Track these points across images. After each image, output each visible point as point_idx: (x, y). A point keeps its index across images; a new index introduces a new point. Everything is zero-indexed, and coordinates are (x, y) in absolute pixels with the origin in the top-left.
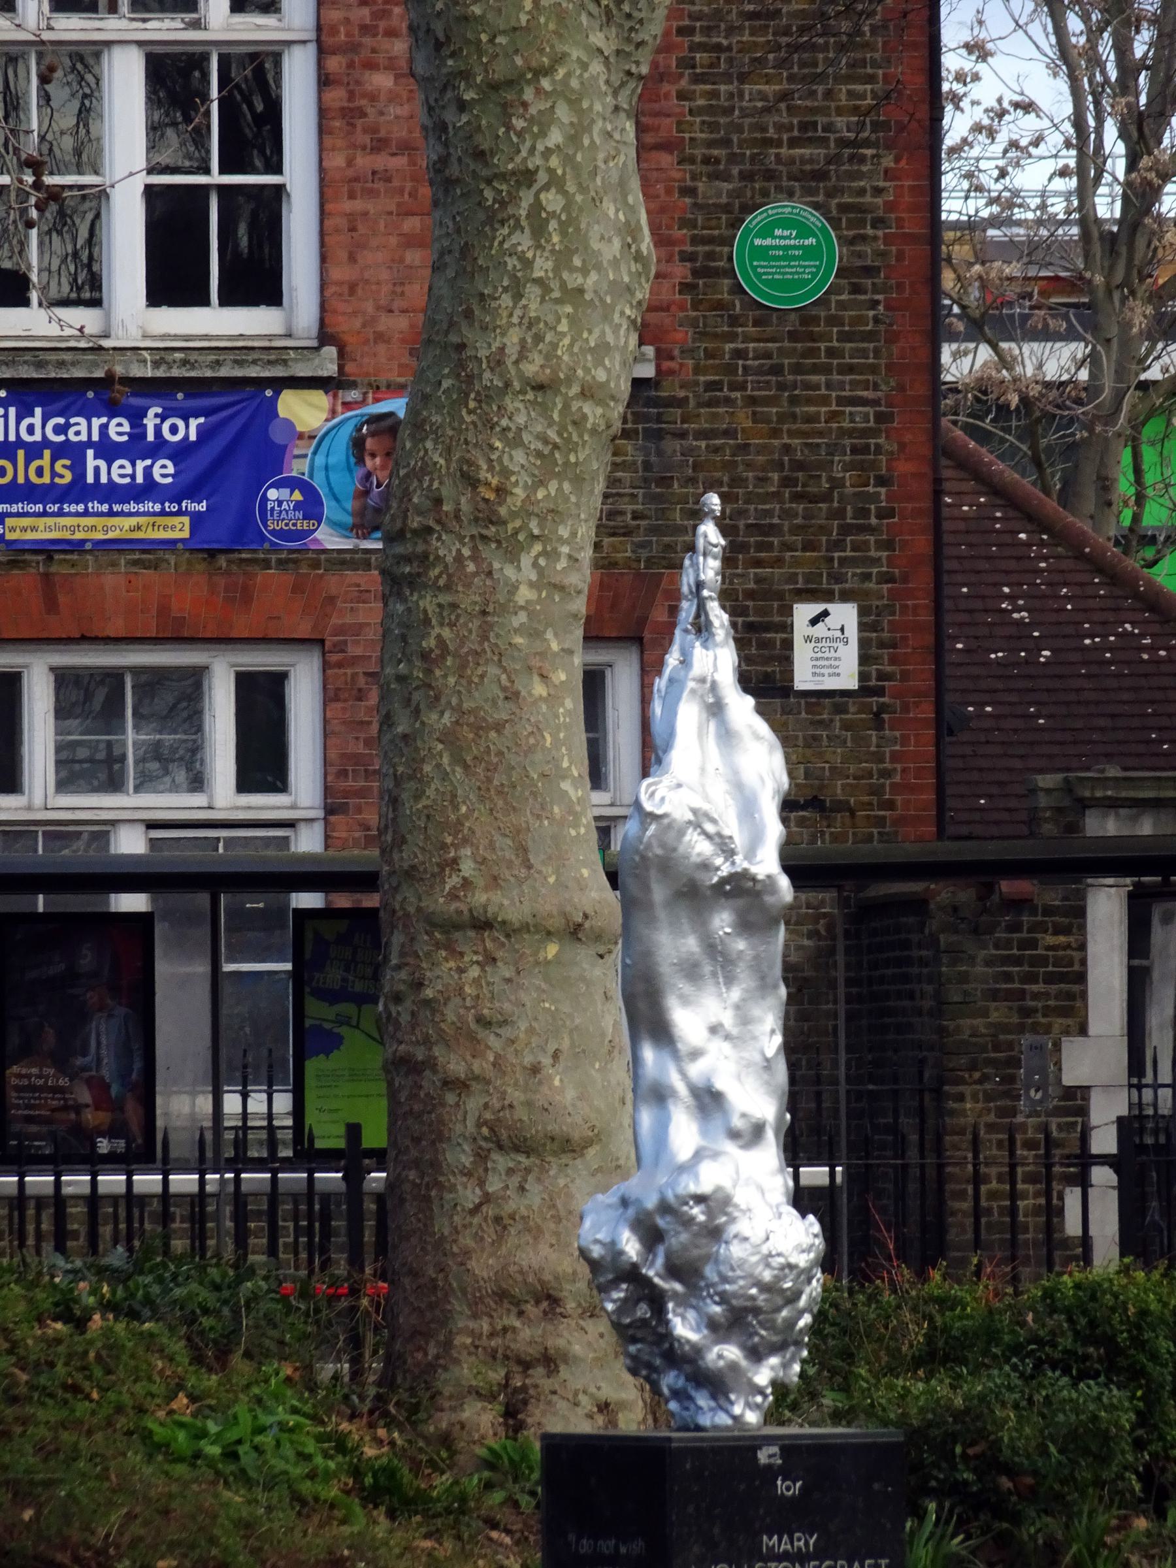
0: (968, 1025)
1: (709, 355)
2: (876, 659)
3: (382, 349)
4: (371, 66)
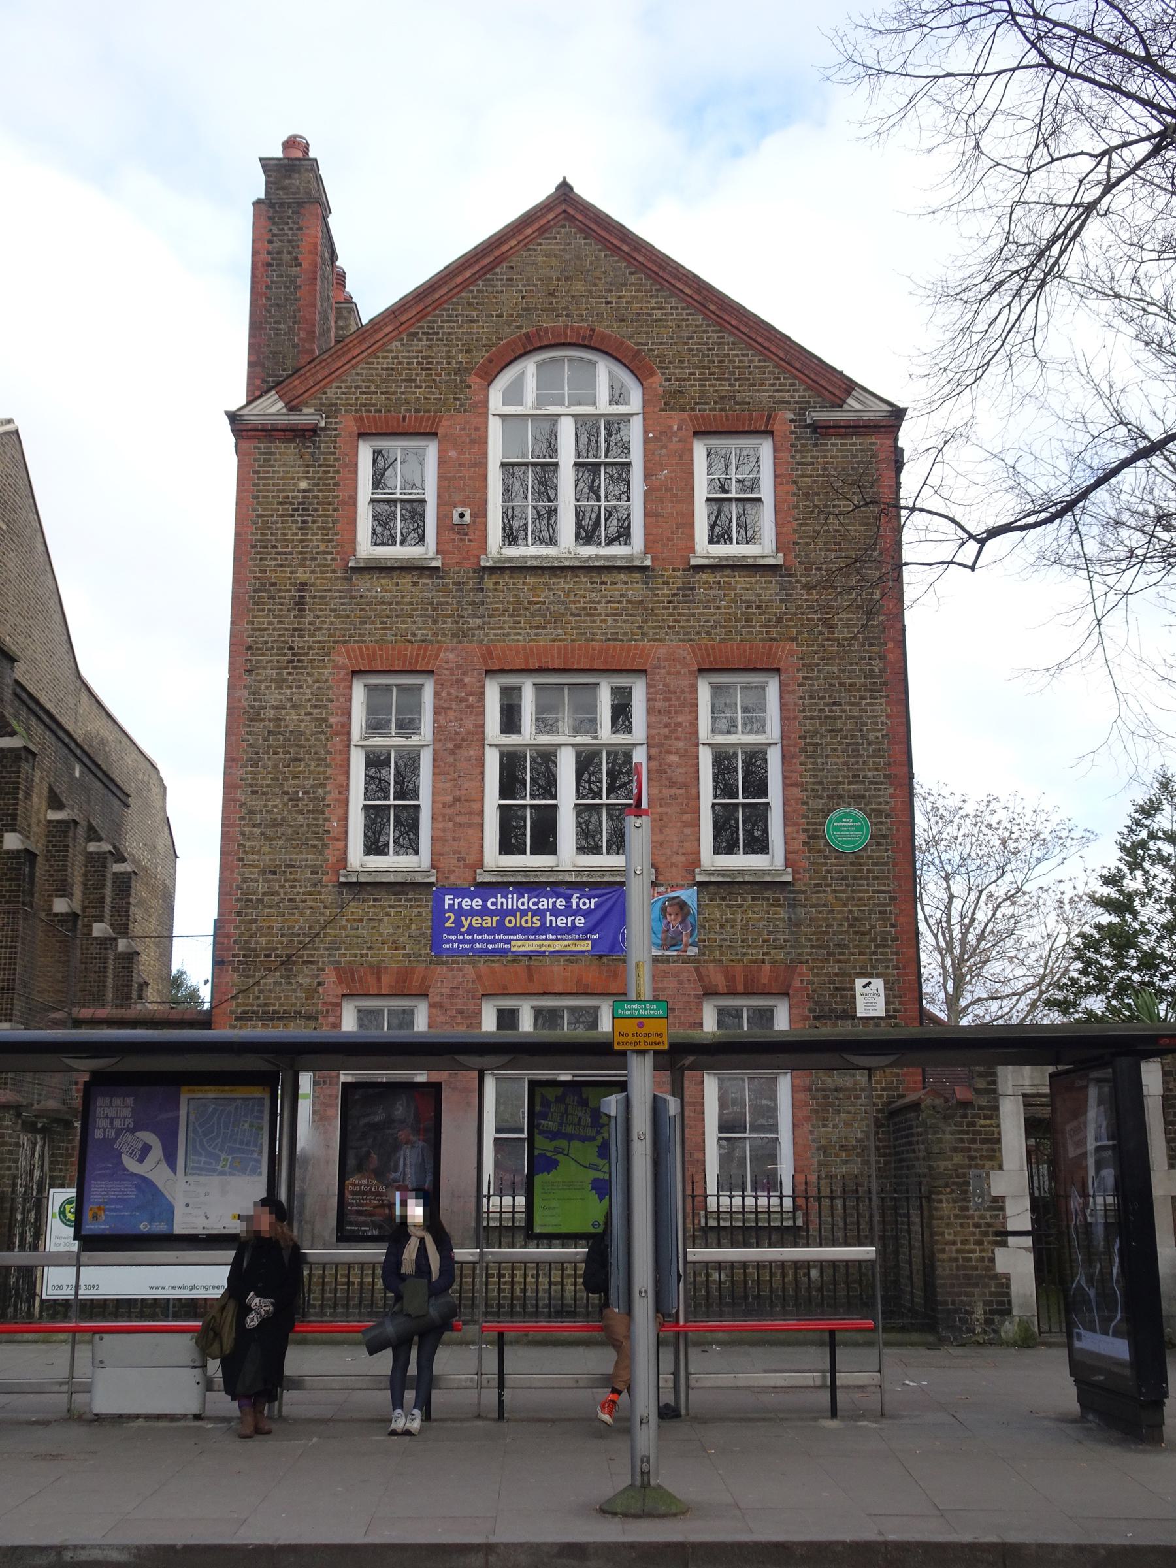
0: (943, 1165)
1: (816, 872)
2: (893, 1003)
3: (674, 870)
4: (669, 752)
